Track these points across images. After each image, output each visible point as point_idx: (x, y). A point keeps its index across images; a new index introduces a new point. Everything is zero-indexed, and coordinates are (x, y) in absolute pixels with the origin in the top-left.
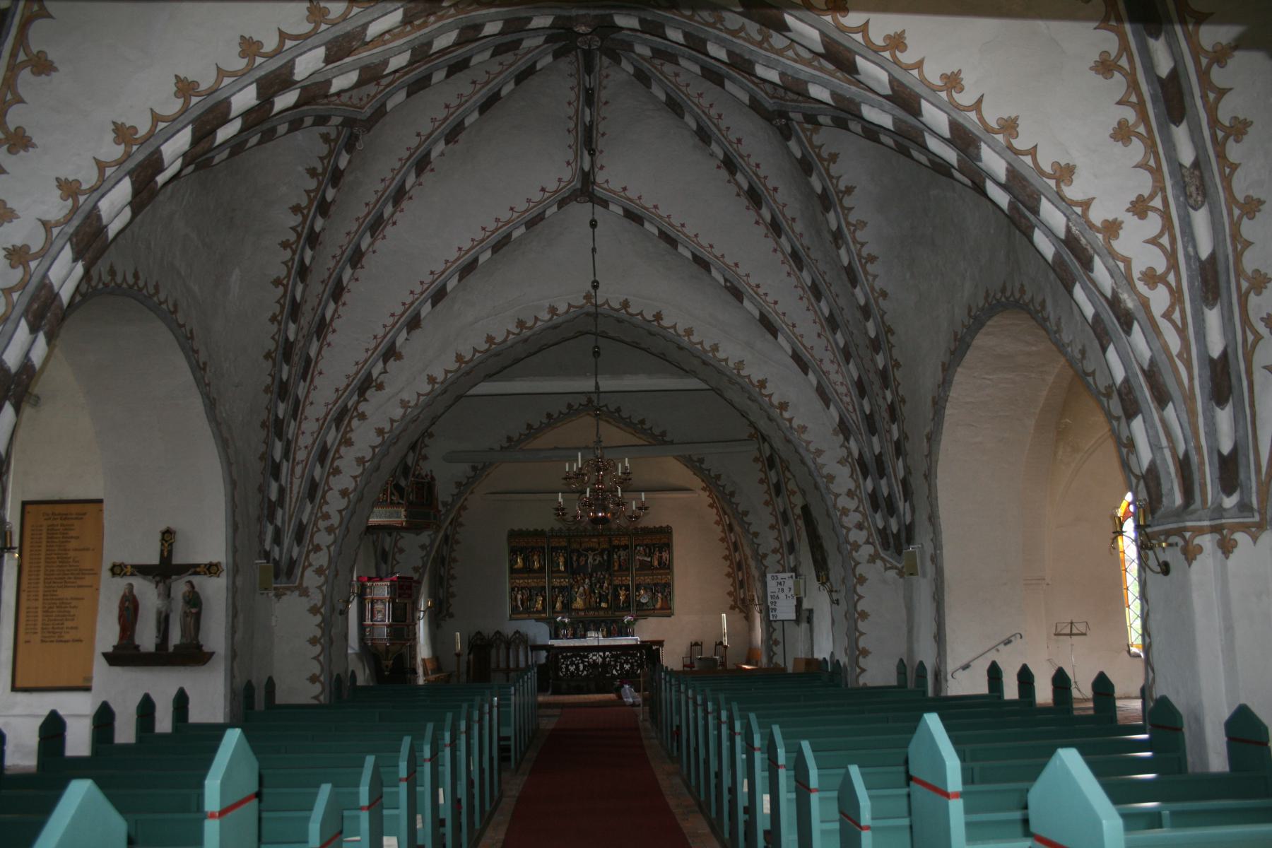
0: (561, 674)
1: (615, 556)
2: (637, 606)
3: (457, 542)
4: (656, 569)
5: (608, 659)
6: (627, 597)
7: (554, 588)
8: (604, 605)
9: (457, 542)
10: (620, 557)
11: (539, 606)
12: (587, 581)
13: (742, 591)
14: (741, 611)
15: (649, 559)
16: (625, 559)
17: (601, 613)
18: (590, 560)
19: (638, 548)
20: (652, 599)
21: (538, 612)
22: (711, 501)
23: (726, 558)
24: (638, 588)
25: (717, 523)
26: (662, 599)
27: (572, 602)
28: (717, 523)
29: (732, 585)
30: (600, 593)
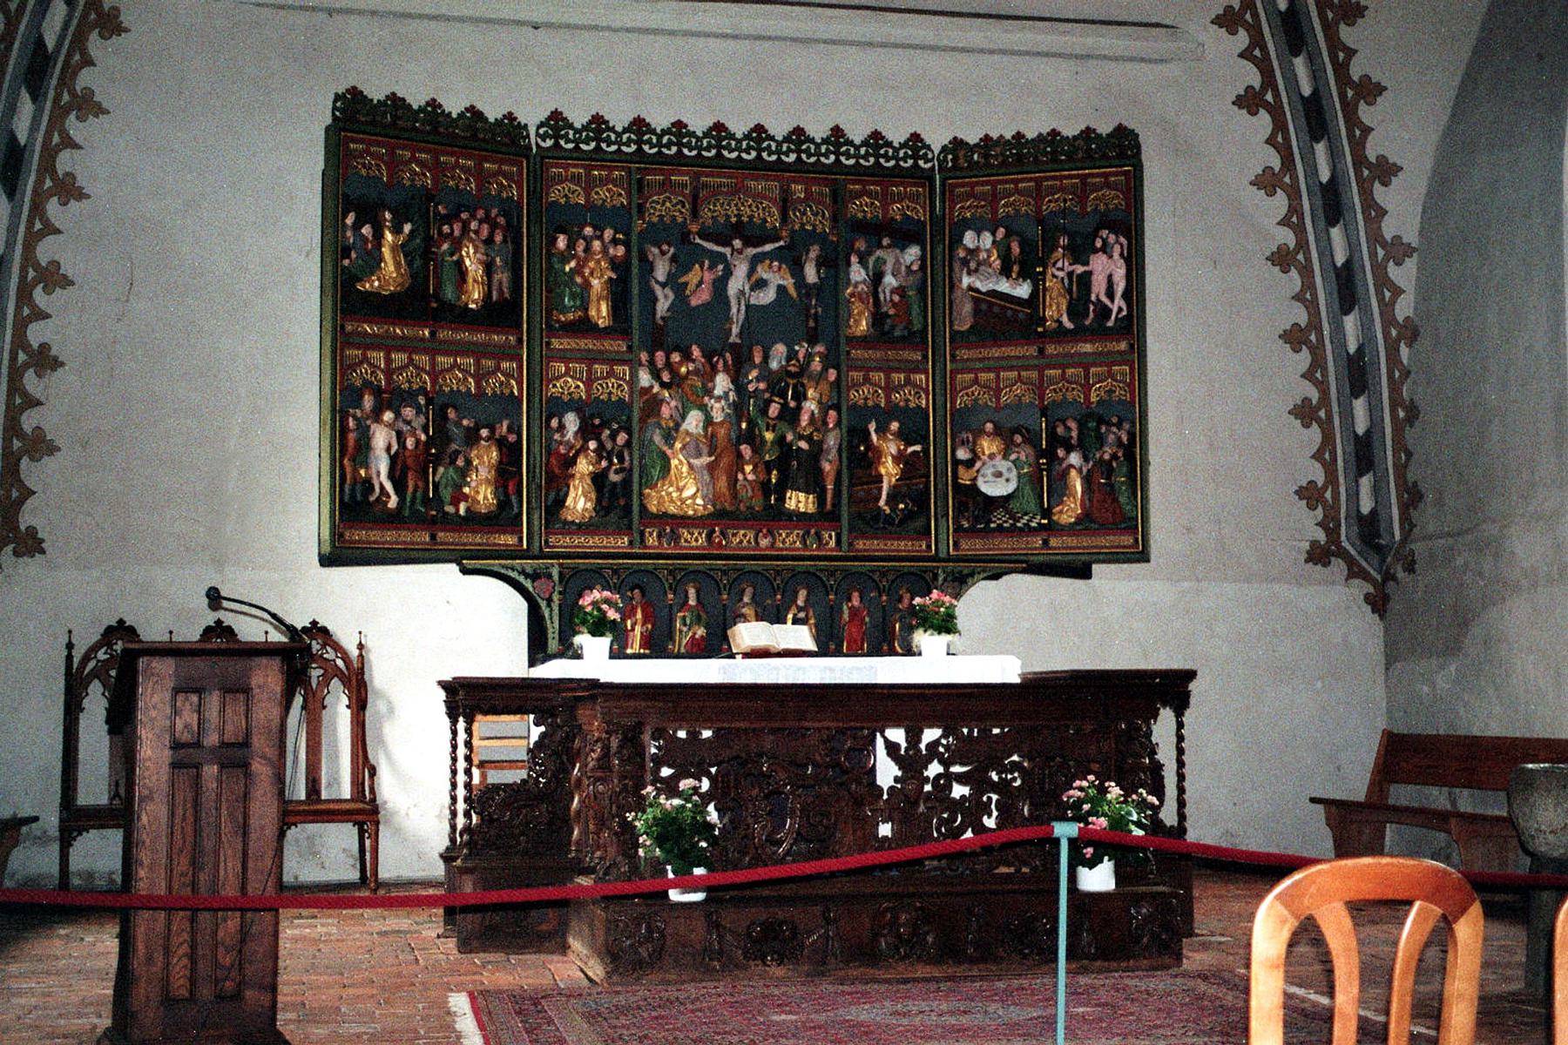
0: (1018, 783)
1: (857, 273)
2: (960, 509)
3: (69, 190)
4: (1060, 334)
5: (934, 769)
6: (910, 465)
7: (557, 407)
8: (799, 501)
9: (69, 190)
10: (877, 278)
11: (482, 492)
12: (722, 383)
13: (1366, 482)
14: (1355, 572)
15: (1023, 290)
16: (900, 290)
17: (789, 540)
18: (737, 283)
19: (969, 239)
20: (1035, 479)
21: (475, 521)
22: (1255, 79)
23: (1294, 338)
24: (965, 424)
25: (1267, 182)
26: (1088, 480)
27: (647, 482)
28: (1267, 182)
29: (1317, 456)
30: (781, 440)
